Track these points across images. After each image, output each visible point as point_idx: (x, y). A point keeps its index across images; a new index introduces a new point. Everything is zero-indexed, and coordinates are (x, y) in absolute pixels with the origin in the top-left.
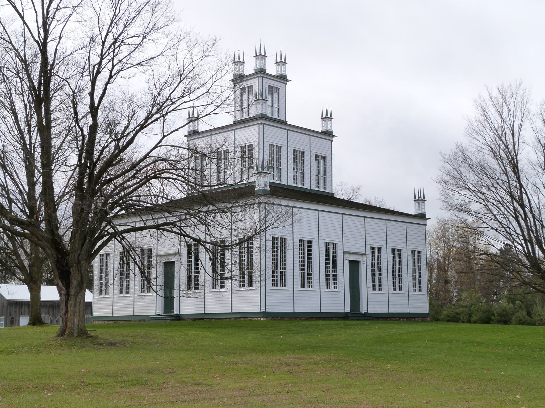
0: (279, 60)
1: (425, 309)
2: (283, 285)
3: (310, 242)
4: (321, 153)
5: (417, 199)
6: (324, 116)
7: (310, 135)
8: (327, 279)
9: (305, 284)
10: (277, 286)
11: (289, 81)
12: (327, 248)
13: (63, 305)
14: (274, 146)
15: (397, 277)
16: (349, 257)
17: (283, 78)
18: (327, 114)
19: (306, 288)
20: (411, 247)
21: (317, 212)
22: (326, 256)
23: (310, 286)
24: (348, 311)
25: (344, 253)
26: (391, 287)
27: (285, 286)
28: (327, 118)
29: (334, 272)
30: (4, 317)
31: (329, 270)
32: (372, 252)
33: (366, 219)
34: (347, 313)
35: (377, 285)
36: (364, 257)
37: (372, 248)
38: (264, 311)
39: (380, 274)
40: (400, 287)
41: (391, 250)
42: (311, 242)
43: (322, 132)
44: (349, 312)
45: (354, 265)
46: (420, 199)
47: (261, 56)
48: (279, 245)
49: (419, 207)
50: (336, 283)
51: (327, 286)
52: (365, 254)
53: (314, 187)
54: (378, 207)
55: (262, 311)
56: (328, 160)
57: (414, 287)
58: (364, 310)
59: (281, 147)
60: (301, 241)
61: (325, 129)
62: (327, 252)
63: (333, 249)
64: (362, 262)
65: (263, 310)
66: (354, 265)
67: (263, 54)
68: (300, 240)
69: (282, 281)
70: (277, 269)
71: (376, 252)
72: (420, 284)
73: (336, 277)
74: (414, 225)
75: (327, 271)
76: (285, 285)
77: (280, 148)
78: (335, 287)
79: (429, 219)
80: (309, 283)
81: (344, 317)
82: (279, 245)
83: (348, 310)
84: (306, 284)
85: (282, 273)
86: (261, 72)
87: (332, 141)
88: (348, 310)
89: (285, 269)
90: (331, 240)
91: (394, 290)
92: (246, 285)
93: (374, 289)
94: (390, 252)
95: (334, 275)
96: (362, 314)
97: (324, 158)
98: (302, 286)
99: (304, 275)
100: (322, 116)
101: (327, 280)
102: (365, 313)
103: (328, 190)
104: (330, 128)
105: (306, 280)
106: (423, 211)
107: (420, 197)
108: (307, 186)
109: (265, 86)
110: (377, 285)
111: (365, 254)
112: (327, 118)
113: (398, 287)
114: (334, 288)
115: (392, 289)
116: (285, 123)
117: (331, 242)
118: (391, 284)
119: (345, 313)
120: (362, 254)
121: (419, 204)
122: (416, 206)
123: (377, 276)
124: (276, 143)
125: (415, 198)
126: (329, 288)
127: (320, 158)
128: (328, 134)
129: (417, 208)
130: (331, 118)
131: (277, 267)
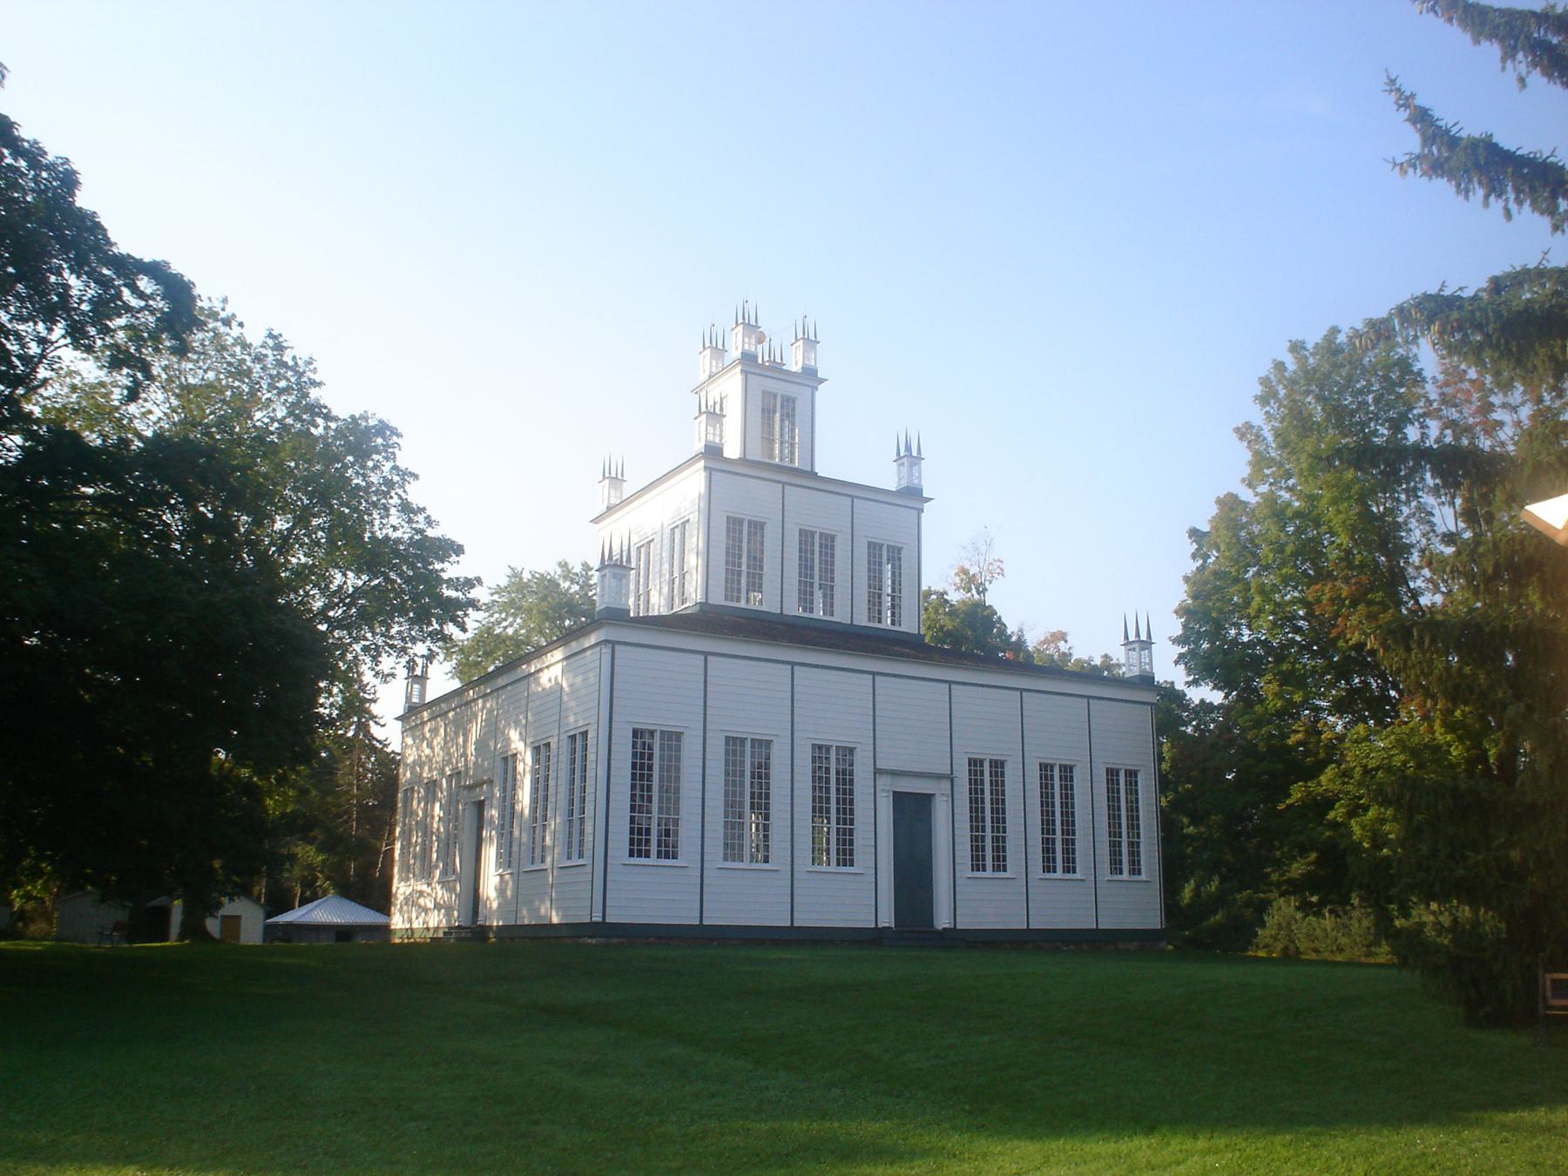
4: (887, 537)
9: (835, 857)
11: (822, 381)
18: (908, 448)
24: (947, 926)
27: (675, 857)
28: (909, 457)
34: (883, 928)
37: (975, 764)
38: (600, 919)
42: (1002, 764)
43: (898, 491)
53: (862, 620)
58: (942, 921)
60: (975, 764)
61: (904, 484)
65: (597, 918)
74: (742, 662)
76: (1005, 866)
81: (871, 938)
83: (887, 919)
88: (887, 919)
89: (1004, 832)
92: (654, 848)
96: (937, 932)
97: (895, 554)
104: (916, 481)
108: (840, 616)
112: (909, 457)
116: (812, 475)
119: (876, 928)
120: (939, 777)
128: (912, 496)
130: (919, 458)
131: (1054, 830)
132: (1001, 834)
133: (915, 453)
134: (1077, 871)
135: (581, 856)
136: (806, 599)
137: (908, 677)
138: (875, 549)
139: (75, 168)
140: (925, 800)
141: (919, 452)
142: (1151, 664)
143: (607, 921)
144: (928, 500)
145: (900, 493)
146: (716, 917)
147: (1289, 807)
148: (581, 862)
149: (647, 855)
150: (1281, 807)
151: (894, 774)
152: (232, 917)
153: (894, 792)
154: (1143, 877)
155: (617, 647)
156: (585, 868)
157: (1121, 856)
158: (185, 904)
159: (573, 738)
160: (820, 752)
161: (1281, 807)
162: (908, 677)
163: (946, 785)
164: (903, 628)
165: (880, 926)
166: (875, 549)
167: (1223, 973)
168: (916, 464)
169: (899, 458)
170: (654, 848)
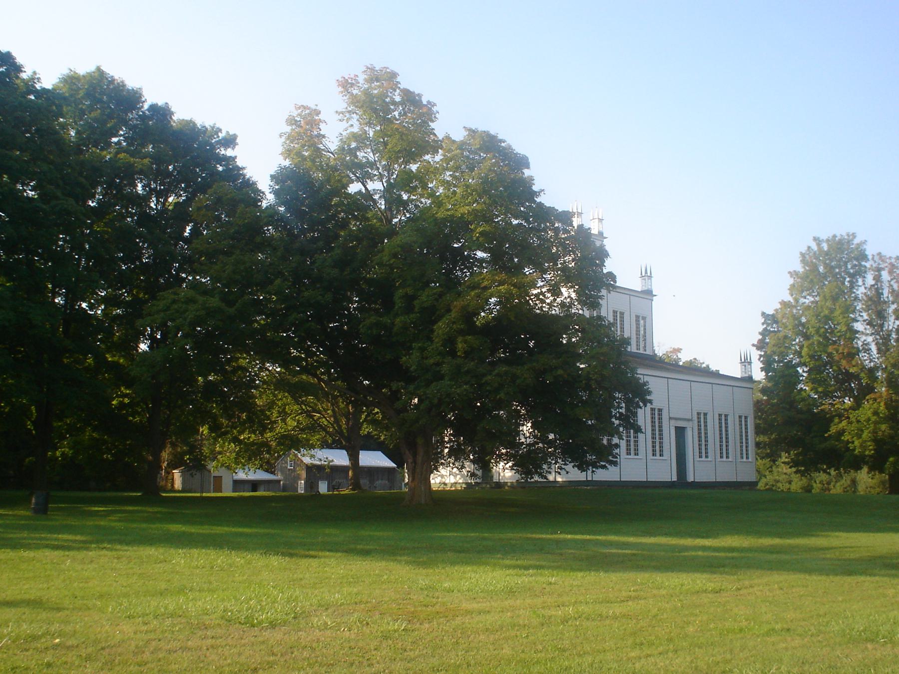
2: (636, 454)
4: (641, 313)
8: (653, 446)
15: (657, 440)
16: (674, 423)
18: (646, 272)
23: (636, 454)
25: (670, 418)
26: (718, 455)
29: (660, 439)
30: (303, 492)
32: (699, 418)
35: (703, 451)
36: (691, 423)
37: (699, 414)
41: (717, 416)
45: (680, 432)
48: (657, 419)
49: (745, 369)
54: (728, 376)
55: (673, 480)
56: (647, 320)
58: (690, 478)
61: (645, 288)
66: (680, 432)
71: (702, 417)
82: (657, 419)
83: (675, 479)
84: (632, 452)
88: (675, 479)
91: (660, 456)
93: (700, 457)
94: (717, 417)
96: (689, 483)
97: (644, 318)
100: (641, 274)
103: (648, 352)
104: (650, 287)
105: (632, 447)
106: (750, 373)
110: (703, 451)
112: (646, 275)
115: (651, 454)
118: (697, 450)
120: (688, 420)
121: (745, 366)
122: (742, 369)
125: (741, 360)
127: (641, 318)
128: (648, 294)
129: (744, 370)
130: (650, 277)
137: (680, 380)
138: (637, 317)
139: (607, 248)
145: (643, 292)
146: (652, 478)
147: (830, 436)
148: (748, 460)
150: (826, 435)
151: (676, 419)
152: (218, 476)
153: (675, 427)
154: (730, 459)
157: (724, 451)
158: (182, 472)
161: (826, 435)
162: (680, 380)
164: (647, 353)
166: (637, 317)
167: (809, 494)
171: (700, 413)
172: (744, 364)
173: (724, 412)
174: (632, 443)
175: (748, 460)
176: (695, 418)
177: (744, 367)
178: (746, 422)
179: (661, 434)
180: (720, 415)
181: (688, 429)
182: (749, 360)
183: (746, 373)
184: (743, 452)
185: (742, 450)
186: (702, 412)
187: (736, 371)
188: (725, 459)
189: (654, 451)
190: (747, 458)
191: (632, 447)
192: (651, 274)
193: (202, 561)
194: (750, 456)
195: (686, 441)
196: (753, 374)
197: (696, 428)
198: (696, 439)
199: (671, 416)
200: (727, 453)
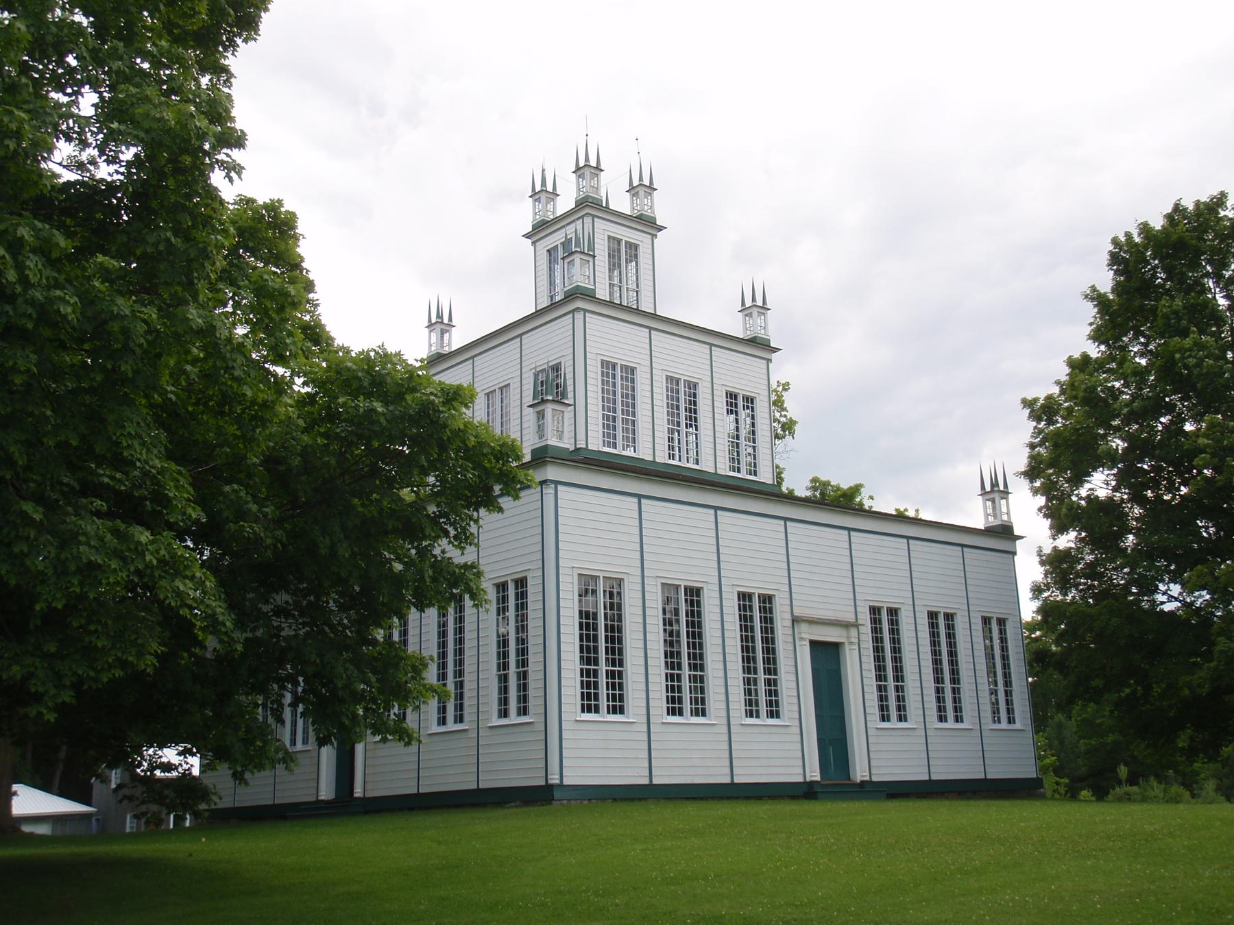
0: (636, 183)
1: (1027, 770)
2: (614, 710)
3: (893, 612)
5: (988, 488)
6: (748, 303)
7: (651, 329)
10: (889, 720)
11: (661, 228)
12: (933, 626)
13: (848, 782)
14: (614, 366)
15: (891, 684)
17: (648, 224)
18: (440, 315)
19: (894, 723)
20: (926, 603)
21: (846, 532)
22: (744, 628)
23: (902, 718)
25: (795, 620)
26: (932, 712)
31: (943, 678)
33: (852, 533)
34: (812, 782)
36: (853, 632)
37: (875, 611)
38: (557, 782)
39: (523, 663)
40: (956, 711)
44: (817, 782)
46: (996, 489)
47: (587, 170)
49: (994, 508)
50: (904, 706)
51: (883, 715)
52: (856, 625)
57: (996, 711)
58: (860, 772)
59: (633, 370)
62: (934, 635)
63: (763, 610)
64: (846, 644)
67: (646, 182)
68: (928, 612)
69: (899, 708)
70: (680, 668)
72: (956, 700)
73: (903, 692)
74: (981, 552)
75: (938, 680)
76: (778, 712)
77: (692, 386)
78: (774, 714)
79: (1021, 537)
80: (770, 704)
81: (805, 792)
83: (814, 774)
85: (897, 689)
86: (589, 205)
87: (769, 361)
88: (814, 774)
90: (757, 587)
91: (901, 720)
92: (603, 703)
93: (942, 719)
94: (924, 622)
95: (953, 689)
98: (590, 706)
99: (755, 684)
101: (882, 701)
102: (863, 782)
106: (1005, 518)
107: (994, 484)
109: (602, 237)
111: (856, 625)
113: (893, 712)
114: (901, 721)
115: (936, 718)
117: (885, 605)
119: (805, 783)
120: (846, 625)
121: (993, 501)
123: (948, 685)
124: (622, 357)
126: (946, 721)
129: (990, 511)
131: (755, 669)
132: (618, 669)
133: (446, 320)
134: (1017, 721)
135: (524, 711)
136: (735, 461)
140: (835, 647)
141: (450, 319)
142: (1008, 514)
143: (565, 783)
144: (776, 350)
148: (442, 729)
149: (597, 711)
151: (812, 622)
154: (1018, 726)
155: (643, 501)
156: (715, 730)
159: (502, 587)
160: (669, 589)
163: (572, 619)
165: (808, 780)
168: (447, 331)
169: (431, 325)
170: (603, 703)
171: (750, 596)
172: (991, 496)
173: (942, 606)
174: (686, 684)
175: (1012, 727)
176: (865, 618)
177: (989, 503)
178: (1002, 632)
179: (955, 672)
180: (932, 615)
181: (847, 647)
182: (1002, 488)
183: (995, 516)
184: (1003, 709)
185: (504, 690)
186: (995, 616)
187: (771, 482)
188: (514, 718)
189: (884, 709)
190: (1011, 720)
191: (686, 695)
192: (764, 302)
193: (1191, 884)
194: (1017, 715)
195: (842, 673)
196: (1013, 520)
197: (868, 644)
198: (871, 675)
199: (797, 612)
200: (1010, 711)
